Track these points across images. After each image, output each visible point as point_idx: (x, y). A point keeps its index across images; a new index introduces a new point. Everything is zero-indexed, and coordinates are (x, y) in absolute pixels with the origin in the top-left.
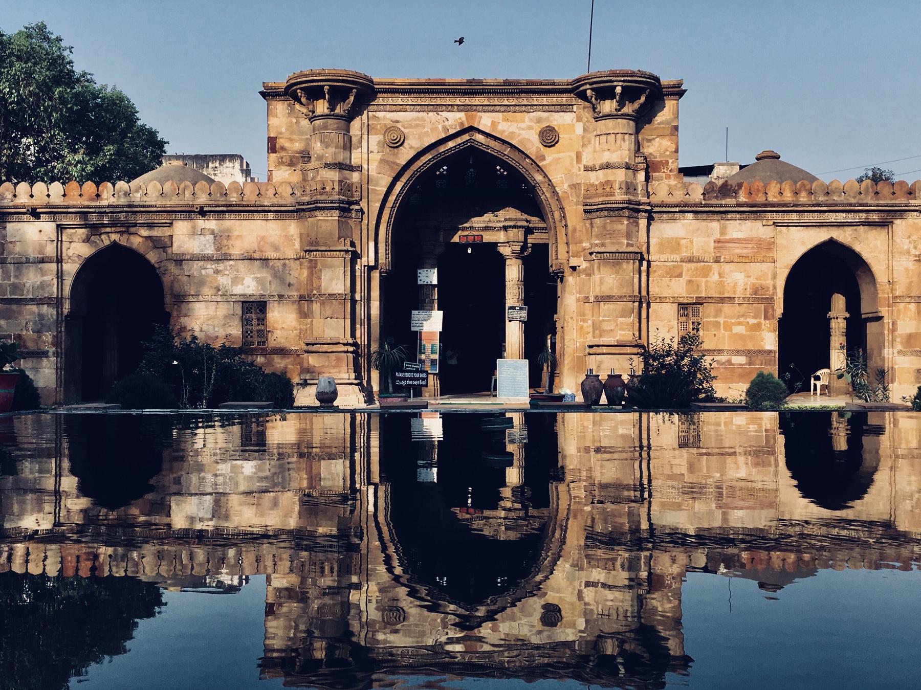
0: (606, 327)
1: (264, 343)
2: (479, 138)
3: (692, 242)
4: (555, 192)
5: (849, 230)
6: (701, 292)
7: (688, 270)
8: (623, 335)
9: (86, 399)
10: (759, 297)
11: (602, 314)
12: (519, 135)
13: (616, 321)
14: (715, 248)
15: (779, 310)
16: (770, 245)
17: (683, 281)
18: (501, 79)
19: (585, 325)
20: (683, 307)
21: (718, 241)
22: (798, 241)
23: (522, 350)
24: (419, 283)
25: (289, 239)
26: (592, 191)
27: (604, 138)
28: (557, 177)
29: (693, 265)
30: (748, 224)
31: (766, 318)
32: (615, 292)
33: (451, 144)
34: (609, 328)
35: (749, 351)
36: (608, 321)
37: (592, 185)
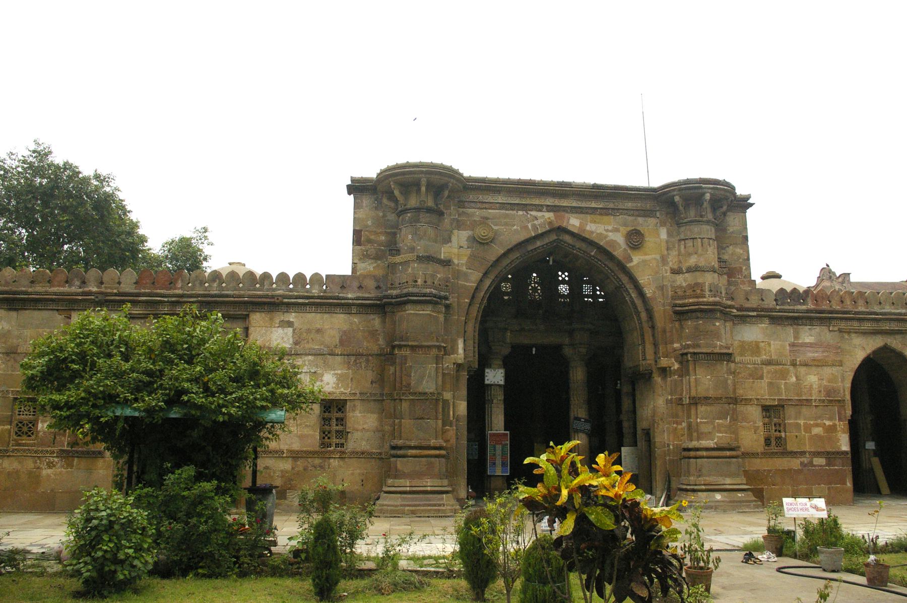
0: (704, 429)
1: (342, 445)
2: (567, 238)
3: (769, 344)
4: (641, 294)
5: (898, 337)
6: (781, 394)
7: (768, 372)
8: (721, 438)
10: (830, 400)
11: (699, 416)
12: (606, 237)
13: (713, 423)
14: (790, 351)
15: (849, 412)
16: (839, 350)
17: (764, 383)
18: (592, 183)
19: (679, 427)
20: (766, 409)
21: (792, 345)
22: (860, 349)
24: (487, 382)
25: (373, 334)
26: (680, 293)
27: (690, 243)
28: (644, 279)
29: (772, 368)
30: (817, 329)
32: (711, 393)
33: (539, 243)
34: (706, 431)
35: (828, 453)
36: (705, 423)
37: (681, 287)
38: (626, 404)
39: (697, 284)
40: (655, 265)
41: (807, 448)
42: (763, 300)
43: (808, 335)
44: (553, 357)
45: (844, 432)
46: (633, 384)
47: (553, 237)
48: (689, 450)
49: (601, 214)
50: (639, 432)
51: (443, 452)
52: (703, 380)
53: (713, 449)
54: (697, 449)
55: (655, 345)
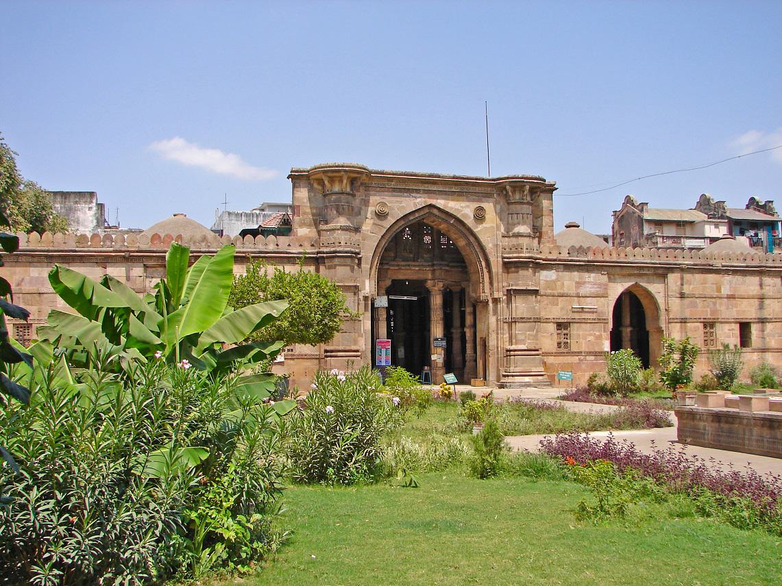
0: (521, 337)
1: (292, 350)
2: (435, 212)
8: (529, 343)
9: (2, 398)
15: (610, 326)
16: (606, 287)
18: (452, 175)
20: (560, 325)
22: (618, 288)
23: (650, 333)
31: (604, 331)
36: (521, 334)
38: (469, 320)
39: (518, 245)
40: (490, 230)
41: (583, 349)
42: (560, 253)
43: (591, 277)
44: (419, 288)
45: (606, 340)
46: (474, 307)
47: (427, 210)
48: (510, 351)
49: (458, 195)
50: (478, 340)
51: (359, 353)
52: (521, 307)
53: (525, 350)
54: (515, 350)
55: (491, 283)
